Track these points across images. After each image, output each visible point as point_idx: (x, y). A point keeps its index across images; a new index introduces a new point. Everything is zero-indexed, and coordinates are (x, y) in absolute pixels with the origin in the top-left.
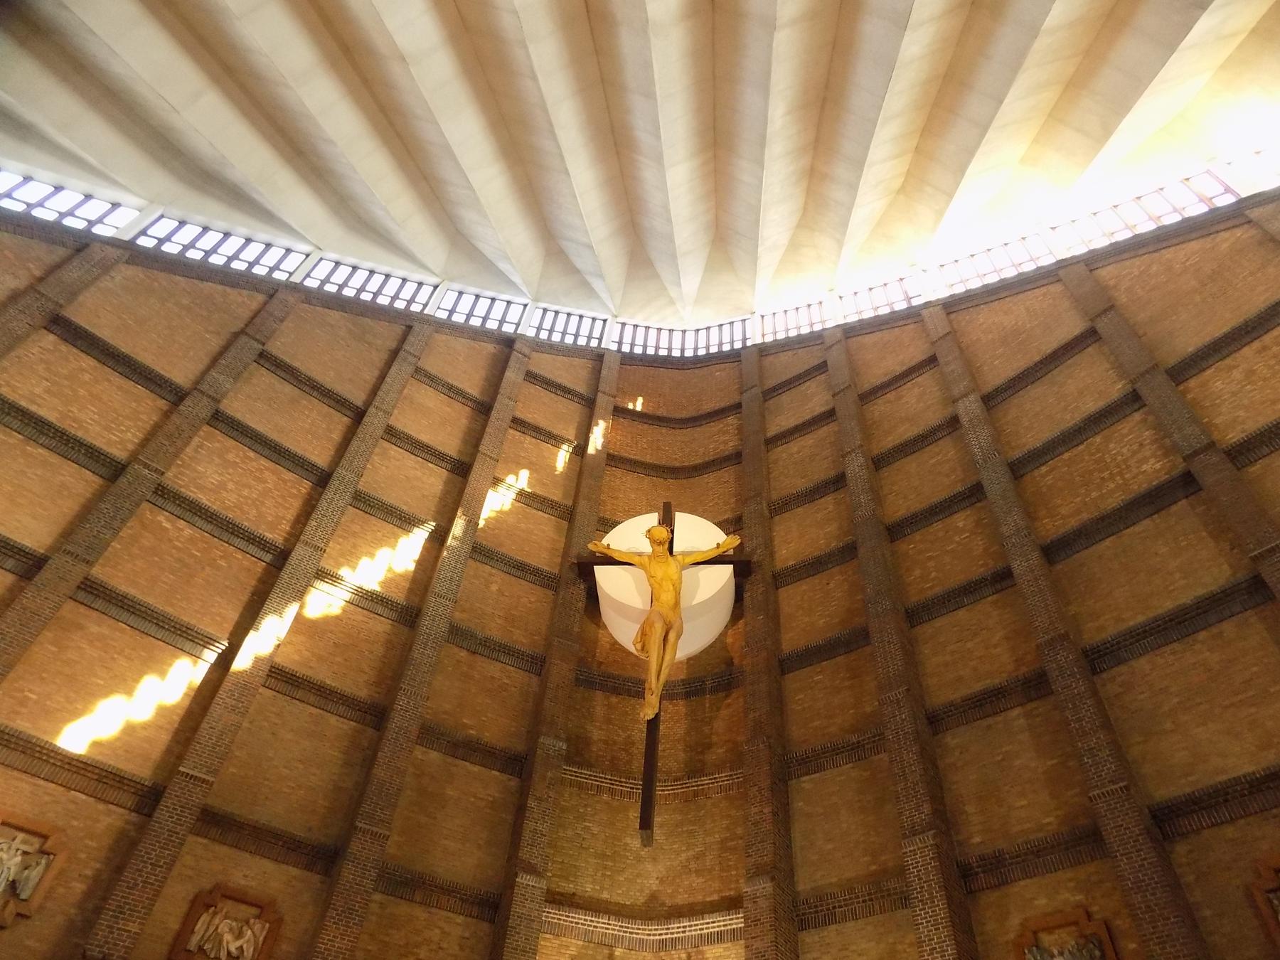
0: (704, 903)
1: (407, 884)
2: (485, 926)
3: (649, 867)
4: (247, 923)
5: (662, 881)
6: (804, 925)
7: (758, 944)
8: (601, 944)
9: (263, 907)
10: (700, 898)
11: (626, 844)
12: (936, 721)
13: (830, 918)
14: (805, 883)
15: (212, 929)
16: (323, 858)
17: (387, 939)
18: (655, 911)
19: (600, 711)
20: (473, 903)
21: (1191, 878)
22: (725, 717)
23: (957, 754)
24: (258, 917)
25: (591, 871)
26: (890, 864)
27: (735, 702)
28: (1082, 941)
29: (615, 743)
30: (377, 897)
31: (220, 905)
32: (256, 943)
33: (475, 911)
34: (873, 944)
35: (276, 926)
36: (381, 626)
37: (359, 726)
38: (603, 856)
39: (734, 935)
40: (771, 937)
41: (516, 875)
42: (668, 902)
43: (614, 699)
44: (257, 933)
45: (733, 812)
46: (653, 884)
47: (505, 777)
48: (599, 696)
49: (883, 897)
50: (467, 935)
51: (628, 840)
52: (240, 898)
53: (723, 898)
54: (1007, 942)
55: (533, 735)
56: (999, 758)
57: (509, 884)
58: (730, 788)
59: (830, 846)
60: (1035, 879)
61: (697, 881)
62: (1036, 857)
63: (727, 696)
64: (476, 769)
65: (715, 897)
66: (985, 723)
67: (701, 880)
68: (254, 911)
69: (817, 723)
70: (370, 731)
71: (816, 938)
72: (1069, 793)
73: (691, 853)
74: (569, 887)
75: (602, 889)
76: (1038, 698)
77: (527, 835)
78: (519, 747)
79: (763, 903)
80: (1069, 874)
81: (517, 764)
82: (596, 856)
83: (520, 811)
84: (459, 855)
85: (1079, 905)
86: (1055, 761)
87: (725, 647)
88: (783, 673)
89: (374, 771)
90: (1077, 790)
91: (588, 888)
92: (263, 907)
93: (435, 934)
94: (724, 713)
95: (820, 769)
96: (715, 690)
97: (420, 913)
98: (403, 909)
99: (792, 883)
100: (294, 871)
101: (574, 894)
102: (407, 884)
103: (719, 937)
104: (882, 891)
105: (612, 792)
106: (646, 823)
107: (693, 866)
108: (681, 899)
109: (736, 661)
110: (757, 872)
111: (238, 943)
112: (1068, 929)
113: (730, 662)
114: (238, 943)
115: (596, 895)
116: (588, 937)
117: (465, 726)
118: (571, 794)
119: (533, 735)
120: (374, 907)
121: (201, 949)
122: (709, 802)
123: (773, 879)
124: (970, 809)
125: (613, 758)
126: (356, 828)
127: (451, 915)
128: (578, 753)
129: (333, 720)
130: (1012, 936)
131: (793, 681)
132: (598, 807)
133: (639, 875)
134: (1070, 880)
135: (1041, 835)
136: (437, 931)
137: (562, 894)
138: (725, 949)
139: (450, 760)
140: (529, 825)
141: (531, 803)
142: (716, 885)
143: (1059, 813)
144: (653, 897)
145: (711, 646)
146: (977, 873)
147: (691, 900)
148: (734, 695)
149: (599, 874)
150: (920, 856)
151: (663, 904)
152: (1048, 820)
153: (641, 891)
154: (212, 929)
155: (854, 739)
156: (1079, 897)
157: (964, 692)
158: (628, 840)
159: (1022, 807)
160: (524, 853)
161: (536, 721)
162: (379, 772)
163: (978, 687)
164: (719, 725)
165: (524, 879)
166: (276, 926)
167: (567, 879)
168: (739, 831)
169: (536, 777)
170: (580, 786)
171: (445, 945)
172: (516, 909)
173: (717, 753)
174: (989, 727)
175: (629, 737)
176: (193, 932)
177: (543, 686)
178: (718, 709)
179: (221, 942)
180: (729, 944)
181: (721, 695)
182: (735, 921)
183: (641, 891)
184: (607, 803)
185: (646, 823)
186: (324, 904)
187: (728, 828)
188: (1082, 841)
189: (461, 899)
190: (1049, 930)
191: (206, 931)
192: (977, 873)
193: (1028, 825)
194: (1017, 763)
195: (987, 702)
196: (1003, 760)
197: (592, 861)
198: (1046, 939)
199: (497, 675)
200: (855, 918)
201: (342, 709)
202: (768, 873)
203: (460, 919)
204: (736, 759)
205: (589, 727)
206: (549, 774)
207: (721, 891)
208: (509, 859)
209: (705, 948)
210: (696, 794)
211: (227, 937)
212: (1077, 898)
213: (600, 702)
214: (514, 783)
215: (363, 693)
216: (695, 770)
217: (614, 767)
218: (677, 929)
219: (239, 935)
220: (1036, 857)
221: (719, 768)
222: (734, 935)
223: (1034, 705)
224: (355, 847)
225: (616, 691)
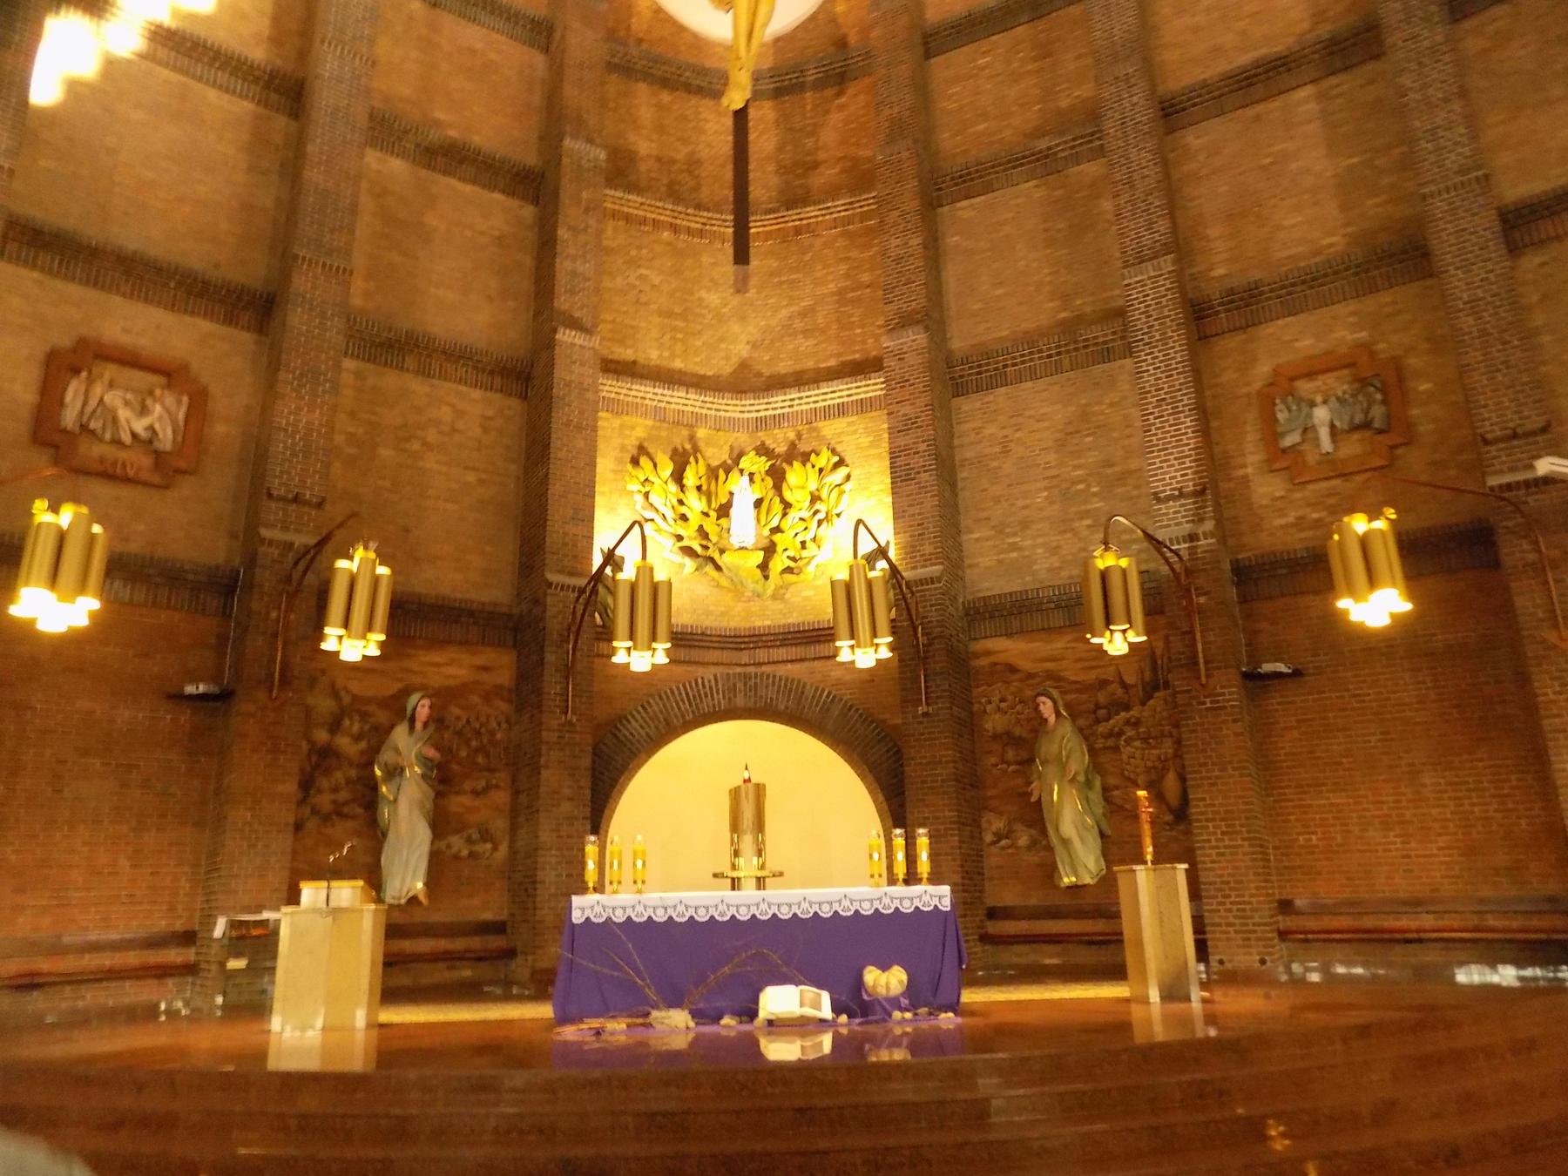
0: (818, 371)
1: (392, 346)
2: (515, 403)
3: (735, 328)
4: (151, 393)
5: (755, 346)
6: (960, 390)
7: (905, 409)
8: (677, 423)
9: (171, 374)
10: (810, 364)
11: (700, 299)
12: (1172, 113)
13: (999, 379)
14: (959, 342)
15: (93, 403)
16: (257, 308)
17: (373, 418)
18: (744, 382)
19: (646, 114)
20: (492, 372)
21: (1535, 298)
22: (838, 125)
23: (1201, 158)
24: (169, 386)
25: (655, 333)
26: (1088, 309)
27: (855, 99)
28: (1356, 386)
29: (673, 161)
30: (349, 364)
31: (96, 370)
32: (174, 422)
33: (498, 381)
34: (1058, 407)
35: (199, 401)
36: (226, 107)
37: (261, 110)
38: (670, 314)
39: (863, 406)
40: (924, 399)
41: (555, 331)
42: (766, 372)
43: (666, 97)
44: (173, 408)
45: (854, 254)
46: (742, 350)
47: (514, 203)
48: (642, 88)
49: (1076, 349)
50: (490, 413)
51: (703, 294)
52: (130, 360)
53: (844, 364)
54: (1248, 395)
55: (551, 139)
56: (1268, 160)
57: (544, 345)
58: (849, 221)
59: (999, 292)
60: (1302, 316)
61: (806, 344)
62: (1304, 288)
63: (839, 94)
64: (467, 189)
65: (832, 362)
66: (1250, 112)
67: (811, 342)
68: (162, 380)
69: (981, 127)
70: (281, 122)
71: (978, 405)
72: (1370, 202)
73: (795, 309)
74: (627, 354)
75: (673, 356)
76: (1345, 69)
77: (562, 280)
78: (530, 158)
79: (913, 360)
80: (1352, 306)
81: (534, 184)
82: (661, 313)
83: (546, 247)
84: (463, 303)
85: (1360, 345)
86: (1355, 160)
87: (833, 20)
88: (928, 55)
89: (307, 174)
90: (1383, 198)
91: (652, 355)
92: (171, 374)
93: (445, 413)
94: (836, 118)
95: (987, 189)
96: (819, 85)
97: (418, 387)
98: (391, 380)
99: (944, 340)
100: (206, 326)
101: (634, 362)
102: (392, 346)
103: (841, 410)
104: (1076, 342)
105: (675, 229)
106: (741, 255)
107: (798, 324)
108: (784, 367)
109: (853, 40)
110: (904, 321)
111: (146, 421)
112: (1336, 374)
113: (842, 44)
114: (146, 421)
115: (664, 363)
116: (659, 414)
117: (437, 124)
118: (615, 229)
119: (551, 139)
120: (347, 378)
121: (84, 428)
122: (818, 243)
123: (927, 329)
124: (1213, 232)
125: (671, 184)
126: (296, 257)
127: (464, 388)
128: (621, 171)
129: (212, 94)
130: (1257, 386)
131: (944, 67)
132: (658, 248)
133: (722, 339)
134: (1352, 314)
135: (1318, 259)
136: (445, 409)
137: (617, 362)
138: (849, 424)
139: (424, 173)
140: (563, 266)
141: (562, 233)
142: (833, 347)
143: (1349, 230)
144: (744, 365)
145: (813, 18)
146: (1218, 313)
147: (798, 367)
148: (850, 91)
149: (667, 337)
150: (1150, 292)
151: (759, 375)
152: (1333, 239)
153: (727, 358)
154: (93, 403)
155: (1042, 144)
156: (1363, 335)
157: (1223, 67)
158: (703, 294)
159: (1293, 226)
160: (562, 302)
161: (554, 120)
162: (314, 175)
163: (1244, 59)
164: (829, 136)
165: (565, 336)
166: (199, 401)
167: (622, 342)
168: (865, 277)
169: (565, 196)
170: (628, 218)
171: (460, 425)
172: (560, 373)
173: (828, 174)
174: (1258, 118)
175: (693, 153)
176: (62, 404)
177: (557, 72)
178: (827, 112)
179: (115, 420)
180: (854, 418)
181: (830, 92)
182: (871, 387)
183: (727, 358)
184: (669, 244)
185: (741, 255)
186: (271, 367)
187: (847, 276)
188: (1400, 257)
189: (475, 368)
190: (1310, 375)
191: (85, 404)
192: (1218, 313)
193: (1301, 249)
194: (1294, 166)
195: (1261, 79)
196: (1272, 164)
197: (656, 320)
198: (1304, 387)
199: (479, 46)
200: (1033, 376)
201: (223, 77)
202: (918, 322)
203: (477, 394)
204: (860, 178)
205: (632, 137)
206: (584, 195)
207: (839, 355)
208: (537, 314)
209: (820, 424)
210: (798, 231)
211: (123, 414)
212: (1356, 336)
213: (645, 101)
214: (528, 211)
215: (258, 54)
216: (793, 199)
217: (679, 189)
218: (780, 403)
219: (143, 411)
220: (1304, 288)
221: (833, 192)
222: (863, 406)
223: (1334, 80)
224: (301, 282)
225: (666, 83)
